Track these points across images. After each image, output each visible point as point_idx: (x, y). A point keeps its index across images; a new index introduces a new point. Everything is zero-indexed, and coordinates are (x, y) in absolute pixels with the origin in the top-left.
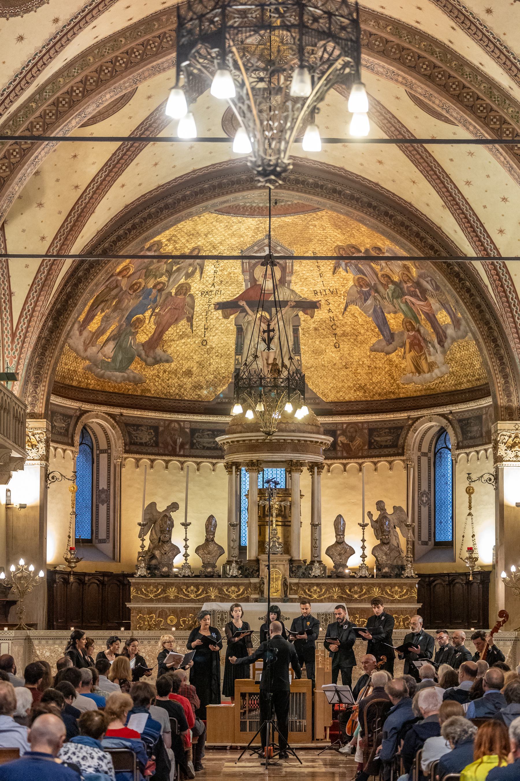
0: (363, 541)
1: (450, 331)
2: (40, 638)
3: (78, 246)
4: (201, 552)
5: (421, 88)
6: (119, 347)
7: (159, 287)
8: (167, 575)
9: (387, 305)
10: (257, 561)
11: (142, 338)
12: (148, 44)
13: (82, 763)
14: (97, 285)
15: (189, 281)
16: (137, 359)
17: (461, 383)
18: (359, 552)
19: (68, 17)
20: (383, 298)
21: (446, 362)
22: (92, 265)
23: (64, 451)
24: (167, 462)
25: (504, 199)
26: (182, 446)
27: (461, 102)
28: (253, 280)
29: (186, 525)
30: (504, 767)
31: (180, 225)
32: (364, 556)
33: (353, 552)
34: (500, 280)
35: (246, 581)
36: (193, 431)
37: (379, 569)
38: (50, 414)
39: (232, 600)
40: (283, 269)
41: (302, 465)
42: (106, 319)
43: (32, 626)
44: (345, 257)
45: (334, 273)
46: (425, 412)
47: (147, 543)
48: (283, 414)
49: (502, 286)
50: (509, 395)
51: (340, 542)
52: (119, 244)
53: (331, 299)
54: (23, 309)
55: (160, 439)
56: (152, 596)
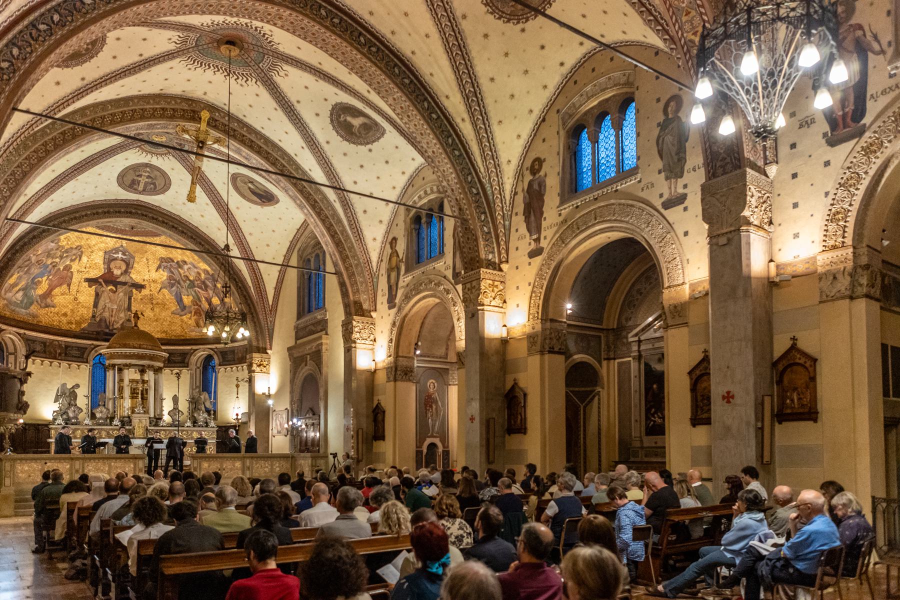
6: (25, 295)
11: (40, 291)
19: (92, 80)
24: (51, 363)
25: (268, 245)
26: (60, 354)
28: (109, 271)
36: (67, 347)
42: (20, 278)
46: (201, 347)
53: (152, 285)
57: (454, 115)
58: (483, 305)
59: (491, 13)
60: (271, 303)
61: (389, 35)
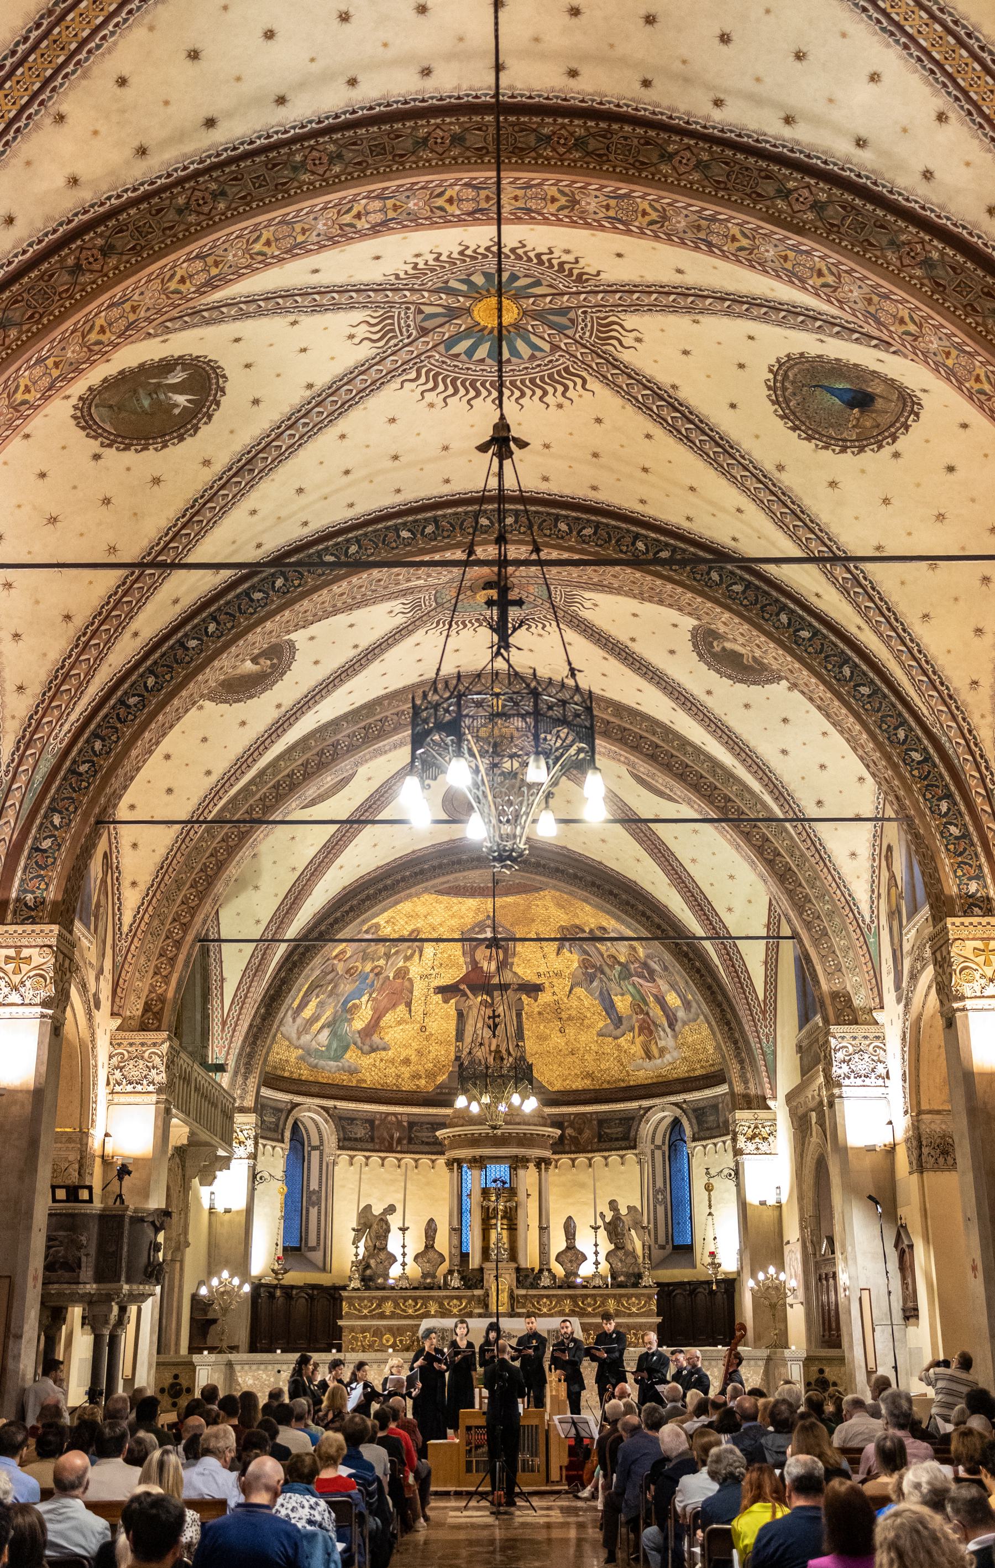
0: (596, 1245)
1: (681, 1014)
2: (243, 1363)
3: (292, 931)
4: (420, 1260)
5: (644, 768)
6: (334, 1034)
7: (376, 971)
8: (383, 1288)
9: (613, 986)
10: (481, 1270)
11: (358, 1024)
12: (370, 727)
13: (292, 1515)
14: (312, 970)
15: (408, 964)
16: (352, 1047)
17: (694, 1070)
18: (591, 1258)
19: (291, 703)
20: (610, 980)
21: (678, 1047)
22: (307, 949)
23: (274, 1148)
25: (731, 877)
26: (399, 1141)
27: (685, 781)
28: (475, 965)
29: (403, 1230)
30: (785, 1517)
31: (399, 907)
32: (597, 1263)
33: (585, 1258)
34: (731, 959)
35: (469, 1293)
36: (411, 1125)
37: (614, 1277)
38: (260, 1107)
39: (455, 1316)
40: (506, 951)
41: (528, 1161)
42: (321, 1005)
43: (233, 1349)
44: (569, 938)
45: (558, 954)
46: (657, 1101)
47: (361, 1251)
48: (510, 1106)
49: (733, 966)
50: (746, 1082)
51: (571, 1247)
52: (336, 927)
54: (235, 995)
55: (376, 1134)
56: (365, 1311)
57: (844, 623)
58: (963, 998)
59: (826, 448)
60: (761, 997)
61: (686, 525)
